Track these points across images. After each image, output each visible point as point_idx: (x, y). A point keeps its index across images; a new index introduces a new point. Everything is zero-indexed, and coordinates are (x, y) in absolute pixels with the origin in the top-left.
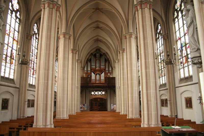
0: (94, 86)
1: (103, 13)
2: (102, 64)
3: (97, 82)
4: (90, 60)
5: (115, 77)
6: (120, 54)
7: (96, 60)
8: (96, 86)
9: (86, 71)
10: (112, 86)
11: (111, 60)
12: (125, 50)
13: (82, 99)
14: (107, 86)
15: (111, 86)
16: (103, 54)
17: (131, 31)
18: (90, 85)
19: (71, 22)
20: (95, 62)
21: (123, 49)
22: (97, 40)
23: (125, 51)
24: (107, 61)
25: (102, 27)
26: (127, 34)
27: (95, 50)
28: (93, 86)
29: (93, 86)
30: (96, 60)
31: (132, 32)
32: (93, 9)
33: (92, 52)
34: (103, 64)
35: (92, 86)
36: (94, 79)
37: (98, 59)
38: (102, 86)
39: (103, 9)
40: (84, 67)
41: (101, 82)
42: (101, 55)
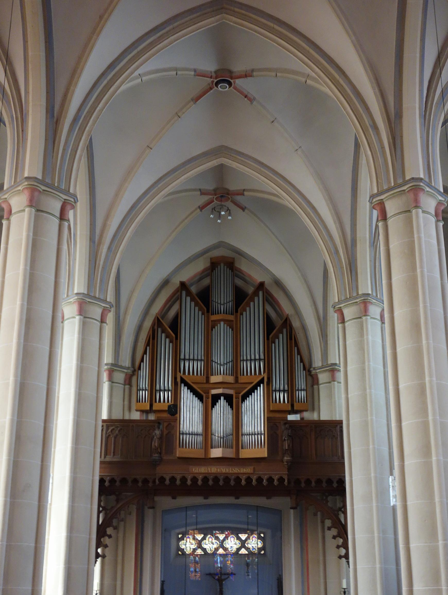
0: (194, 479)
1: (243, 209)
2: (245, 352)
3: (216, 453)
4: (175, 325)
5: (341, 422)
6: (390, 222)
7: (210, 327)
8: (205, 479)
9: (144, 394)
10: (319, 481)
11: (304, 328)
12: (339, 371)
13: (115, 579)
14: (281, 480)
15: (308, 482)
16: (256, 293)
17: (366, 286)
18: (167, 471)
19: (109, 248)
20: (201, 338)
21: (364, 295)
22: (222, 196)
23: (340, 376)
24: (282, 330)
25: (241, 193)
26: (346, 300)
27: (201, 266)
28: (189, 478)
29: (189, 478)
30: (210, 327)
31: (422, 176)
32: (203, 193)
33: (186, 276)
34: (253, 346)
35: (184, 479)
36: (199, 428)
37: (225, 321)
38: (249, 480)
39: (246, 193)
40: (136, 369)
41: (244, 454)
42: (241, 298)
